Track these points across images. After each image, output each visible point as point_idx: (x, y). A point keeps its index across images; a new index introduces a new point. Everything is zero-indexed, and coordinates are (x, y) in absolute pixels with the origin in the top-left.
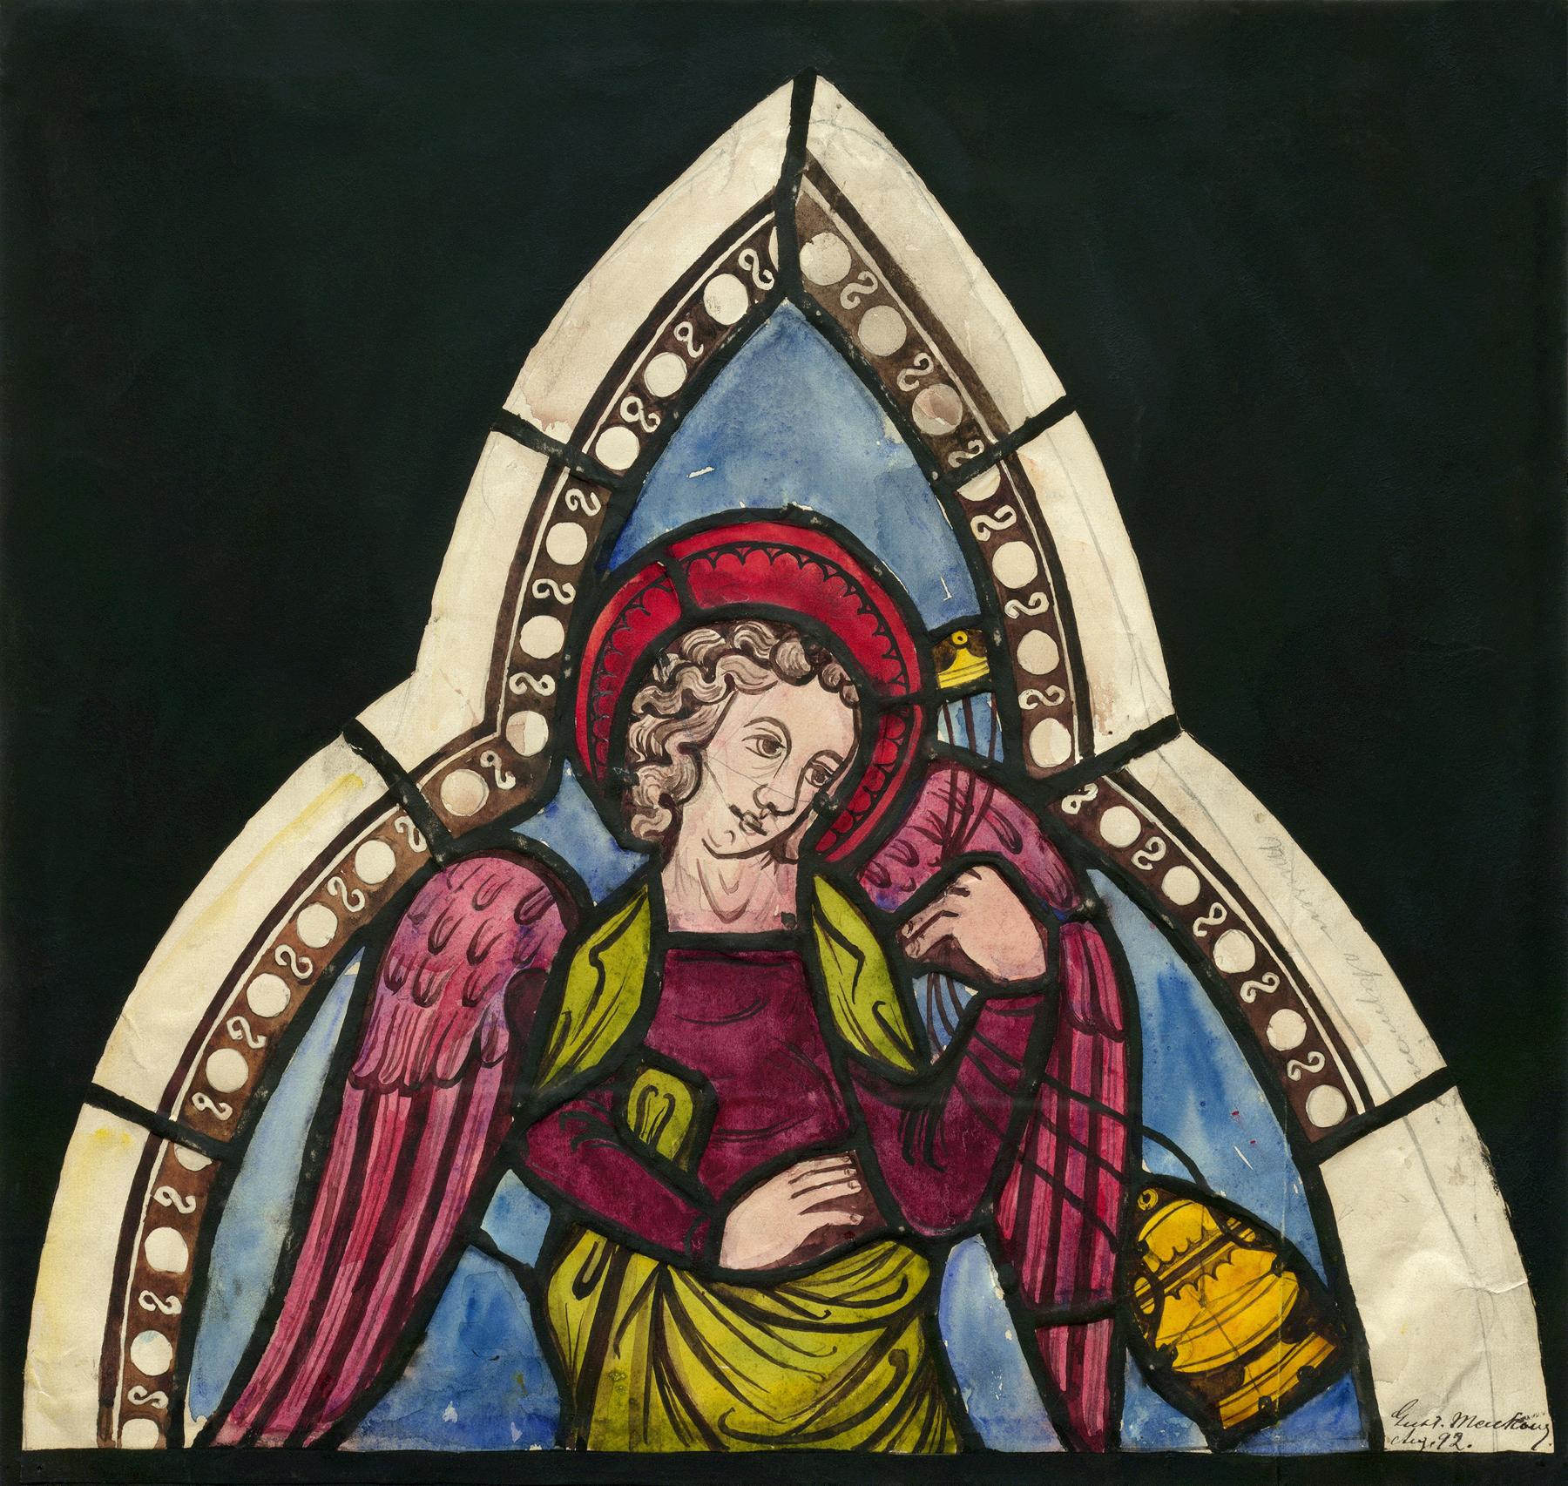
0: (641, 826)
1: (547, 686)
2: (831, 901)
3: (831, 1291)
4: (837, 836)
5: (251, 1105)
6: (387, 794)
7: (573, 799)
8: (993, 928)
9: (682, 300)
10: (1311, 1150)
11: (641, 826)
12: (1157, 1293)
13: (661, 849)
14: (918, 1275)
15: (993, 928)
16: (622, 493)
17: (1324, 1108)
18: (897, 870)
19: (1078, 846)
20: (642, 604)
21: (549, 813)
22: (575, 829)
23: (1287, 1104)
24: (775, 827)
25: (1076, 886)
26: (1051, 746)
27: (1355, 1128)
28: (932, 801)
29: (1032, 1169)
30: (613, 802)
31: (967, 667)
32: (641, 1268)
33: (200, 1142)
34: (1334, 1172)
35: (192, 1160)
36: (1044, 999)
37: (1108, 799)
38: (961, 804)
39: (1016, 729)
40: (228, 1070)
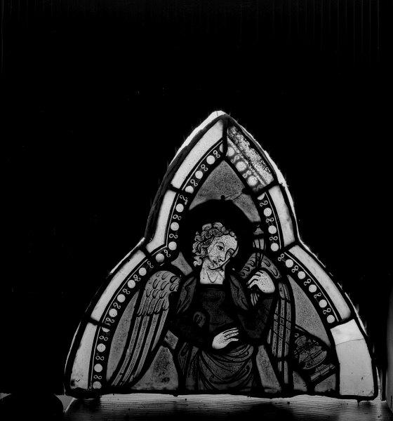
0: (195, 263)
1: (176, 237)
2: (233, 278)
3: (236, 354)
4: (234, 266)
5: (117, 318)
6: (142, 251)
7: (181, 257)
8: (265, 283)
9: (203, 161)
10: (328, 327)
11: (195, 263)
12: (298, 354)
13: (199, 268)
14: (251, 351)
15: (265, 283)
16: (191, 197)
17: (331, 319)
18: (245, 272)
19: (281, 266)
20: (191, 225)
21: (153, 388)
22: (180, 262)
23: (324, 318)
24: (221, 263)
25: (283, 276)
26: (275, 247)
27: (335, 324)
28: (253, 258)
29: (273, 332)
30: (190, 258)
31: (259, 231)
32: (195, 350)
33: (107, 329)
34: (332, 330)
35: (106, 330)
36: (275, 296)
37: (287, 258)
38: (259, 260)
39: (268, 244)
40: (113, 313)
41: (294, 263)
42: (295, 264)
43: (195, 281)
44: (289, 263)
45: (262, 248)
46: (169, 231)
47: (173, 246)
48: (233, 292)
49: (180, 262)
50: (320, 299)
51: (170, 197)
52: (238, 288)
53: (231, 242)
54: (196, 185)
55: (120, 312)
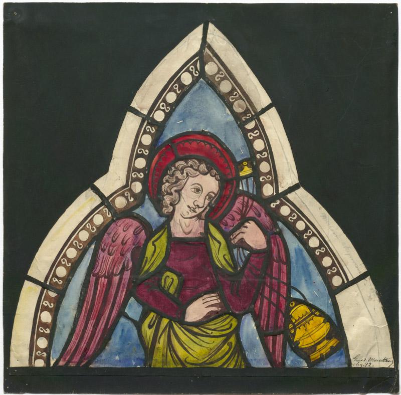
1: (141, 175)
3: (213, 327)
4: (215, 212)
5: (67, 280)
7: (148, 204)
9: (175, 78)
10: (333, 292)
12: (295, 328)
13: (170, 216)
16: (160, 127)
17: (337, 281)
18: (229, 221)
19: (275, 215)
20: (166, 155)
22: (148, 211)
23: (327, 280)
26: (268, 190)
28: (238, 204)
30: (158, 205)
31: (247, 171)
32: (165, 321)
35: (52, 294)
36: (266, 254)
37: (282, 204)
39: (259, 186)
40: (62, 272)
41: (292, 210)
42: (292, 211)
43: (166, 233)
44: (285, 211)
45: (251, 191)
46: (131, 168)
47: (138, 187)
48: (214, 246)
49: (148, 211)
50: (45, 325)
51: (131, 123)
52: (219, 242)
53: (211, 184)
54: (168, 110)
55: (72, 271)
